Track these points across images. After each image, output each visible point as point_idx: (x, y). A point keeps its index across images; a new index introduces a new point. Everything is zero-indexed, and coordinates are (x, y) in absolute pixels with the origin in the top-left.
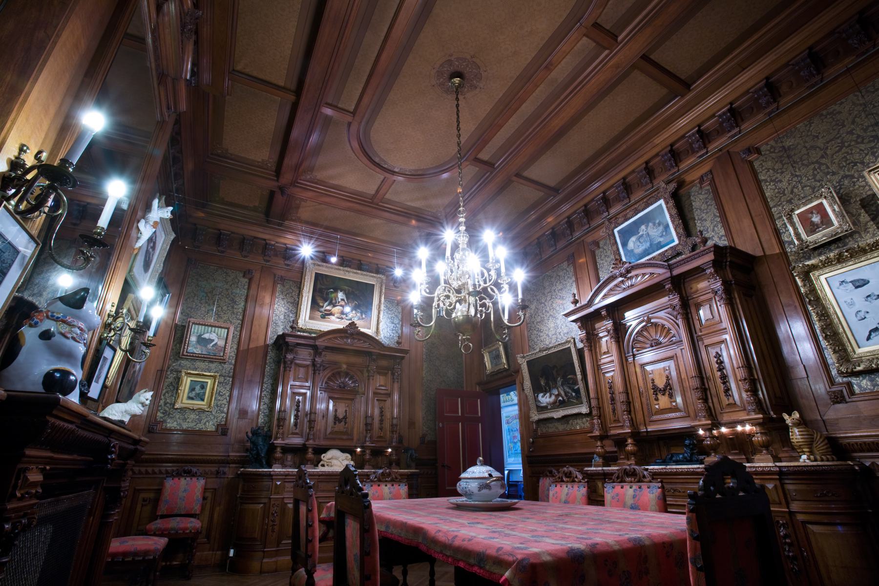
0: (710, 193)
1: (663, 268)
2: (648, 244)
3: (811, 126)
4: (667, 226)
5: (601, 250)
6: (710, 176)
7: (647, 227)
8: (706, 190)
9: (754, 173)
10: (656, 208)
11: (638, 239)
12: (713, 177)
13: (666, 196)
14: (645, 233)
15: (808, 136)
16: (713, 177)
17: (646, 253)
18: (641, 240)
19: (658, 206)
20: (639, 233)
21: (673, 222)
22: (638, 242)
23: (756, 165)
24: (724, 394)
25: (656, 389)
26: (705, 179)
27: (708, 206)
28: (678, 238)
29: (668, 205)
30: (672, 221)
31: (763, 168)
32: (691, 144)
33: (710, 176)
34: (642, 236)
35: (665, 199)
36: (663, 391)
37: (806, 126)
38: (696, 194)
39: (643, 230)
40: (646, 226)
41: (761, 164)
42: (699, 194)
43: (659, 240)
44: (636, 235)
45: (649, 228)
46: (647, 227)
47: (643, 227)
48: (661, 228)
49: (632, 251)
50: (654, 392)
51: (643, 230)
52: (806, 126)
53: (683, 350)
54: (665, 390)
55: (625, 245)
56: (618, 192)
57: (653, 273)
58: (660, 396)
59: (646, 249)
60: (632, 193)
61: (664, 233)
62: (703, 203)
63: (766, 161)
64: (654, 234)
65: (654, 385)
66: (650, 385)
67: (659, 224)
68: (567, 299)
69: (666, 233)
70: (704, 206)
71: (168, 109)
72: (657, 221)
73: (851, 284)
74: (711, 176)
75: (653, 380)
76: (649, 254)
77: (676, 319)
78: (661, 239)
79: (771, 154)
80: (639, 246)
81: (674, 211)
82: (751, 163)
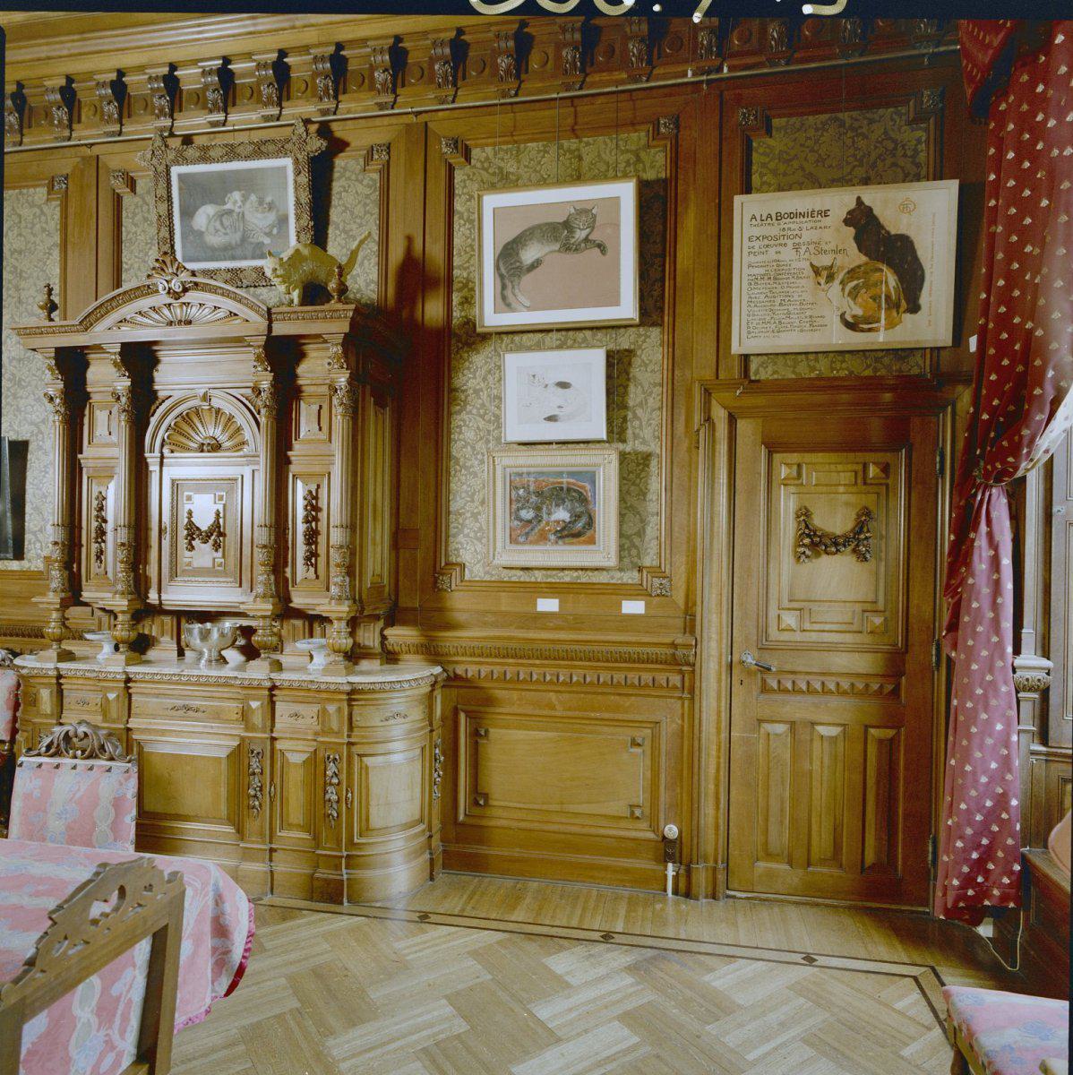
0: (375, 191)
1: (257, 312)
2: (237, 237)
3: (543, 157)
4: (283, 220)
5: (137, 199)
6: (385, 157)
7: (245, 199)
8: (371, 179)
9: (450, 191)
10: (272, 169)
11: (221, 216)
12: (388, 162)
13: (299, 156)
14: (237, 210)
15: (535, 171)
16: (388, 162)
17: (226, 252)
18: (226, 221)
19: (278, 168)
20: (225, 203)
21: (298, 218)
22: (218, 222)
23: (459, 176)
24: (303, 562)
25: (192, 530)
26: (376, 157)
27: (366, 213)
28: (260, 158)
29: (299, 179)
30: (296, 214)
31: (465, 190)
32: (372, 69)
33: (385, 157)
34: (230, 212)
35: (296, 161)
36: (206, 537)
37: (539, 151)
38: (353, 177)
39: (235, 202)
40: (243, 196)
41: (464, 181)
42: (357, 180)
43: (261, 239)
44: (216, 203)
45: (248, 205)
46: (245, 199)
47: (237, 195)
48: (271, 217)
49: (201, 234)
50: (188, 535)
51: (235, 202)
52: (539, 151)
53: (256, 473)
54: (209, 535)
55: (187, 214)
56: (206, 87)
57: (236, 315)
58: (196, 543)
59: (230, 244)
60: (234, 105)
61: (275, 231)
62: (359, 202)
63: (472, 180)
64: (256, 222)
65: (190, 523)
66: (184, 521)
67: (271, 207)
68: (31, 280)
69: (279, 232)
70: (359, 210)
71: (189, 323)
72: (268, 199)
73: (830, 264)
74: (387, 157)
75: (190, 513)
76: (233, 258)
77: (259, 413)
78: (267, 241)
79: (482, 172)
80: (217, 231)
81: (305, 197)
82: (451, 170)
